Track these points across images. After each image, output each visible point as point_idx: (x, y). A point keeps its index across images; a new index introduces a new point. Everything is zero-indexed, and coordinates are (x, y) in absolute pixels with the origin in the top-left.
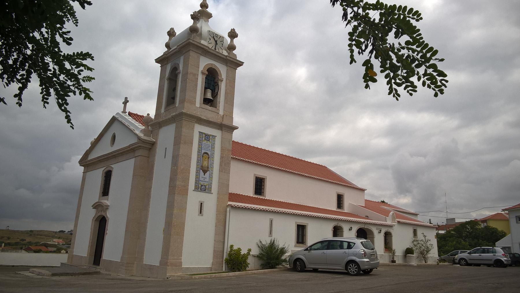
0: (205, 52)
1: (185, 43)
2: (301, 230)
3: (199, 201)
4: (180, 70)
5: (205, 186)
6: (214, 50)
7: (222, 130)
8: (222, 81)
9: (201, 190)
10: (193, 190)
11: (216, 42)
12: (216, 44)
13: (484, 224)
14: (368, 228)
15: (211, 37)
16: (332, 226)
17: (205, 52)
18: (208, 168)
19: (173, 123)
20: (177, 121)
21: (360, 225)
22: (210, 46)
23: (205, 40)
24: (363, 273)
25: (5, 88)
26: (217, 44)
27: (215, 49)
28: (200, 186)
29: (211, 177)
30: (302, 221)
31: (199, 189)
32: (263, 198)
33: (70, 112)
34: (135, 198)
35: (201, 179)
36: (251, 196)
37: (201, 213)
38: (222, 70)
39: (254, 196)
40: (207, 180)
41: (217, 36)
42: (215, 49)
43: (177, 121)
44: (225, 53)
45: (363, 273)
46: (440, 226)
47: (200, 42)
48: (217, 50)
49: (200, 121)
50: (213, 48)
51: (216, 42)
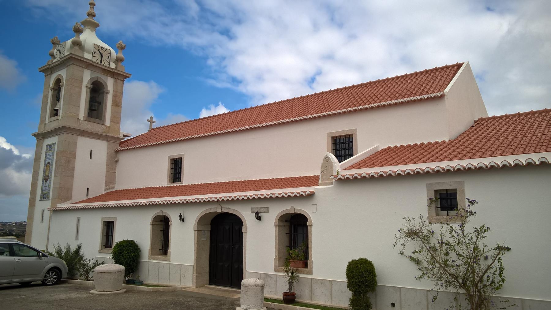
0: (89, 65)
1: (68, 57)
2: (109, 226)
4: (63, 83)
5: (46, 194)
7: (107, 141)
8: (108, 93)
9: (44, 199)
10: (40, 200)
11: (101, 54)
12: (102, 57)
13: (449, 211)
15: (96, 51)
17: (89, 65)
18: (49, 176)
19: (57, 136)
20: (109, 141)
22: (94, 60)
23: (89, 52)
24: (20, 285)
25: (91, 158)
26: (103, 57)
27: (101, 61)
28: (43, 195)
29: (50, 185)
30: (109, 216)
31: (43, 198)
34: (421, 218)
35: (44, 189)
36: (166, 186)
37: (42, 220)
38: (110, 83)
39: (169, 186)
40: (47, 187)
41: (102, 48)
42: (101, 61)
43: (109, 141)
44: (113, 66)
45: (20, 285)
47: (83, 56)
48: (103, 63)
50: (99, 61)
51: (101, 54)
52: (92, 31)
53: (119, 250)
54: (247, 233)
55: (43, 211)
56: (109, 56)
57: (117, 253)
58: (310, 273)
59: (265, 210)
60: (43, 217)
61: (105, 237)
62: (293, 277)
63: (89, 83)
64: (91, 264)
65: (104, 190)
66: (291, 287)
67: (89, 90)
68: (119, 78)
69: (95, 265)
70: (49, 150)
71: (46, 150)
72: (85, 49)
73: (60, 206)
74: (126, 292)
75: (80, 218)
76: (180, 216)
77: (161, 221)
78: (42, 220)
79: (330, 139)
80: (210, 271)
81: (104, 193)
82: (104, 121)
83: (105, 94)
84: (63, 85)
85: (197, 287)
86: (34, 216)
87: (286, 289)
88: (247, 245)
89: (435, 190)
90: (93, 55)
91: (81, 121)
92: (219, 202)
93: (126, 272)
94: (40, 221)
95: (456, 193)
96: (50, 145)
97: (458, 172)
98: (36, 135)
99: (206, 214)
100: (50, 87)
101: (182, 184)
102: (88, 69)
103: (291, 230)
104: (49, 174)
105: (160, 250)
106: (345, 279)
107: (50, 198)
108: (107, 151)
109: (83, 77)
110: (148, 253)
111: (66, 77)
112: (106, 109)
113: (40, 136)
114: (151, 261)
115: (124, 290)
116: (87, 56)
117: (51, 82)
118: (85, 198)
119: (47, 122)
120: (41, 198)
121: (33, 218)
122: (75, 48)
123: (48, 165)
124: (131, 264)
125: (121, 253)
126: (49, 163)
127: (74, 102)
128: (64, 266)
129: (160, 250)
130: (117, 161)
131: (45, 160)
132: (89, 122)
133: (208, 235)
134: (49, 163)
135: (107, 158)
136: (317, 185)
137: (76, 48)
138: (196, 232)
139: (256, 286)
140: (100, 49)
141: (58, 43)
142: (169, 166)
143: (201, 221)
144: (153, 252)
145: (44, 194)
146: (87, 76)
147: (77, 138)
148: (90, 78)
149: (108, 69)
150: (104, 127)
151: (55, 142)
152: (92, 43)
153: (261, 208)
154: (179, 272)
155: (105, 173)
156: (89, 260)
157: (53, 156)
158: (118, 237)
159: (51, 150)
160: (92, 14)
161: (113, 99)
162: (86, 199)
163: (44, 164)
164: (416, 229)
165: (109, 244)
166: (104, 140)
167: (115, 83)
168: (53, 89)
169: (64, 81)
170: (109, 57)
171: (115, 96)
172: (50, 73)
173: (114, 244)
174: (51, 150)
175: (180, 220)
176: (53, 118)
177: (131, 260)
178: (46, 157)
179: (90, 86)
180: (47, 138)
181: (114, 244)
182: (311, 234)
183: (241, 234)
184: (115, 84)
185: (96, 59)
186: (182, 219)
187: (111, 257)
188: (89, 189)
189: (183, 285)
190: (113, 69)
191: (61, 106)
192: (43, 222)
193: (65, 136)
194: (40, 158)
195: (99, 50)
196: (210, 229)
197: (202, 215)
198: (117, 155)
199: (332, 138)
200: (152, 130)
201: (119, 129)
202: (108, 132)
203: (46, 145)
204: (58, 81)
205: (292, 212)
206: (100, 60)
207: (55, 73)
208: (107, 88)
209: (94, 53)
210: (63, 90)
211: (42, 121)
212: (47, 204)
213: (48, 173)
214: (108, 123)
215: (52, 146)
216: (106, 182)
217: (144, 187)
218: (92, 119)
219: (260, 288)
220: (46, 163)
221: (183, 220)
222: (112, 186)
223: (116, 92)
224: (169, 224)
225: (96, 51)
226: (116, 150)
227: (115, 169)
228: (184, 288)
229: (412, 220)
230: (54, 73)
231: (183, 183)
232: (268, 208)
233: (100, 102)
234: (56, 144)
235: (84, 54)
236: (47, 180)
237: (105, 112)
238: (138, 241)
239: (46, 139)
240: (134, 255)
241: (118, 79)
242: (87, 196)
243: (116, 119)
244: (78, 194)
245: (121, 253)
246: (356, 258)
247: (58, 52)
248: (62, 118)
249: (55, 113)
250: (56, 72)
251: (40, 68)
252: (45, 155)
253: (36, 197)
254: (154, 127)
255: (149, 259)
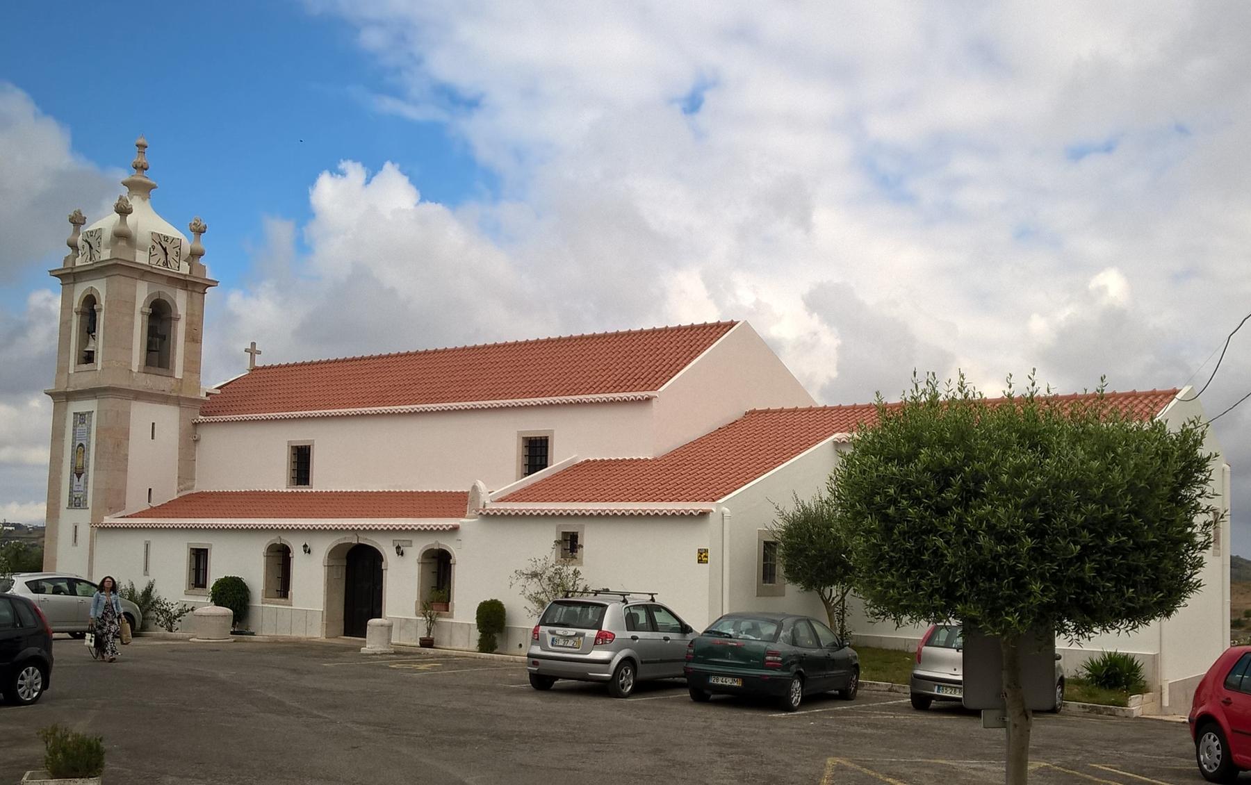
0: (144, 273)
2: (199, 557)
3: (74, 524)
5: (80, 498)
6: (1221, 556)
7: (179, 405)
9: (75, 506)
10: (67, 508)
11: (165, 249)
14: (365, 543)
15: (155, 244)
16: (265, 544)
18: (83, 468)
21: (339, 538)
22: (153, 262)
25: (153, 438)
27: (166, 263)
28: (74, 499)
29: (86, 483)
30: (200, 541)
31: (73, 505)
32: (309, 491)
33: (1209, 454)
35: (75, 489)
36: (285, 491)
37: (75, 542)
38: (180, 301)
39: (290, 491)
42: (166, 263)
44: (185, 269)
46: (686, 694)
48: (194, 274)
49: (139, 395)
51: (165, 249)
52: (144, 199)
53: (221, 590)
54: (456, 566)
55: (76, 527)
56: (179, 251)
57: (218, 594)
58: (451, 617)
59: (407, 543)
60: (76, 536)
61: (193, 573)
62: (432, 621)
63: (146, 304)
64: (174, 610)
65: (176, 492)
66: (429, 630)
67: (146, 318)
68: (196, 290)
69: (181, 613)
70: (80, 423)
71: (75, 422)
72: (137, 243)
73: (108, 520)
74: (235, 641)
75: (149, 541)
76: (305, 546)
77: (279, 551)
78: (75, 542)
79: (521, 440)
80: (345, 619)
81: (176, 497)
82: (173, 371)
83: (173, 321)
84: (100, 310)
85: (326, 638)
86: (58, 535)
87: (423, 634)
88: (186, 566)
89: (563, 533)
90: (150, 253)
91: (134, 374)
92: (355, 531)
93: (234, 616)
94: (71, 542)
95: (577, 536)
96: (82, 415)
97: (583, 516)
98: (53, 395)
99: (339, 545)
100: (74, 307)
101: (311, 490)
102: (143, 280)
103: (439, 568)
104: (83, 464)
105: (277, 591)
106: (475, 622)
107: (89, 504)
108: (178, 423)
109: (135, 296)
110: (261, 595)
111: (106, 297)
112: (175, 348)
113: (61, 397)
114: (266, 605)
115: (233, 640)
116: (142, 258)
117: (75, 298)
118: (145, 506)
119: (71, 371)
120: (69, 504)
121: (57, 538)
122: (119, 244)
123: (80, 449)
124: (238, 609)
125: (223, 594)
126: (81, 445)
127: (120, 342)
128: (137, 612)
129: (277, 591)
130: (196, 441)
131: (74, 439)
132: (149, 375)
133: (342, 572)
134: (81, 445)
135: (180, 435)
136: (463, 516)
137: (122, 243)
138: (326, 568)
139: (382, 626)
140: (163, 240)
141: (82, 222)
142: (290, 457)
143: (334, 553)
144: (267, 594)
145: (76, 498)
146: (142, 293)
147: (130, 405)
148: (146, 296)
149: (178, 277)
150: (173, 380)
151: (91, 410)
152: (149, 230)
153: (404, 541)
154: (304, 619)
155: (177, 462)
156: (172, 605)
157: (89, 433)
158: (216, 573)
159: (84, 423)
160: (142, 167)
161: (186, 329)
162: (149, 508)
163: (72, 446)
164: (539, 570)
165: (201, 582)
166: (174, 404)
167: (190, 298)
168: (82, 313)
169: (102, 301)
170: (177, 253)
171: (189, 324)
172: (72, 281)
173: (211, 582)
174: (84, 423)
175: (305, 551)
176: (85, 367)
177: (237, 605)
178: (74, 434)
179: (148, 310)
180: (75, 400)
181: (211, 582)
182: (454, 573)
183: (381, 572)
184: (190, 302)
185: (157, 262)
186: (307, 550)
187: (209, 601)
188: (152, 490)
189: (309, 635)
190: (186, 275)
191: (99, 345)
192: (76, 546)
193: (111, 402)
194: (63, 435)
195: (162, 243)
196: (345, 564)
197: (334, 545)
198: (196, 430)
199: (525, 439)
200: (254, 369)
201: (199, 383)
202: (180, 390)
203: (74, 413)
204: (90, 301)
205: (436, 548)
206: (163, 259)
207: (82, 282)
208: (177, 310)
209: (152, 249)
210: (101, 319)
211: (62, 369)
212: (83, 518)
213: (81, 465)
214: (179, 374)
215: (87, 416)
216: (179, 477)
217: (248, 490)
218: (152, 369)
219: (387, 628)
220: (77, 445)
221: (309, 552)
222: (190, 484)
223: (192, 315)
224: (291, 555)
225: (155, 244)
226: (195, 420)
227: (194, 455)
228: (311, 638)
229: (538, 561)
230: (78, 282)
231: (312, 488)
232: (411, 541)
233: (165, 336)
234: (94, 416)
235: (136, 252)
236: (81, 474)
237: (173, 355)
238: (246, 579)
239: (73, 402)
240: (241, 597)
241: (195, 291)
242: (149, 502)
243: (193, 365)
244: (136, 500)
245: (223, 594)
246: (488, 599)
247: (87, 246)
248: (102, 368)
249: (89, 358)
250: (84, 281)
251: (53, 271)
252: (73, 430)
253: (59, 502)
254: (258, 364)
255: (262, 603)
